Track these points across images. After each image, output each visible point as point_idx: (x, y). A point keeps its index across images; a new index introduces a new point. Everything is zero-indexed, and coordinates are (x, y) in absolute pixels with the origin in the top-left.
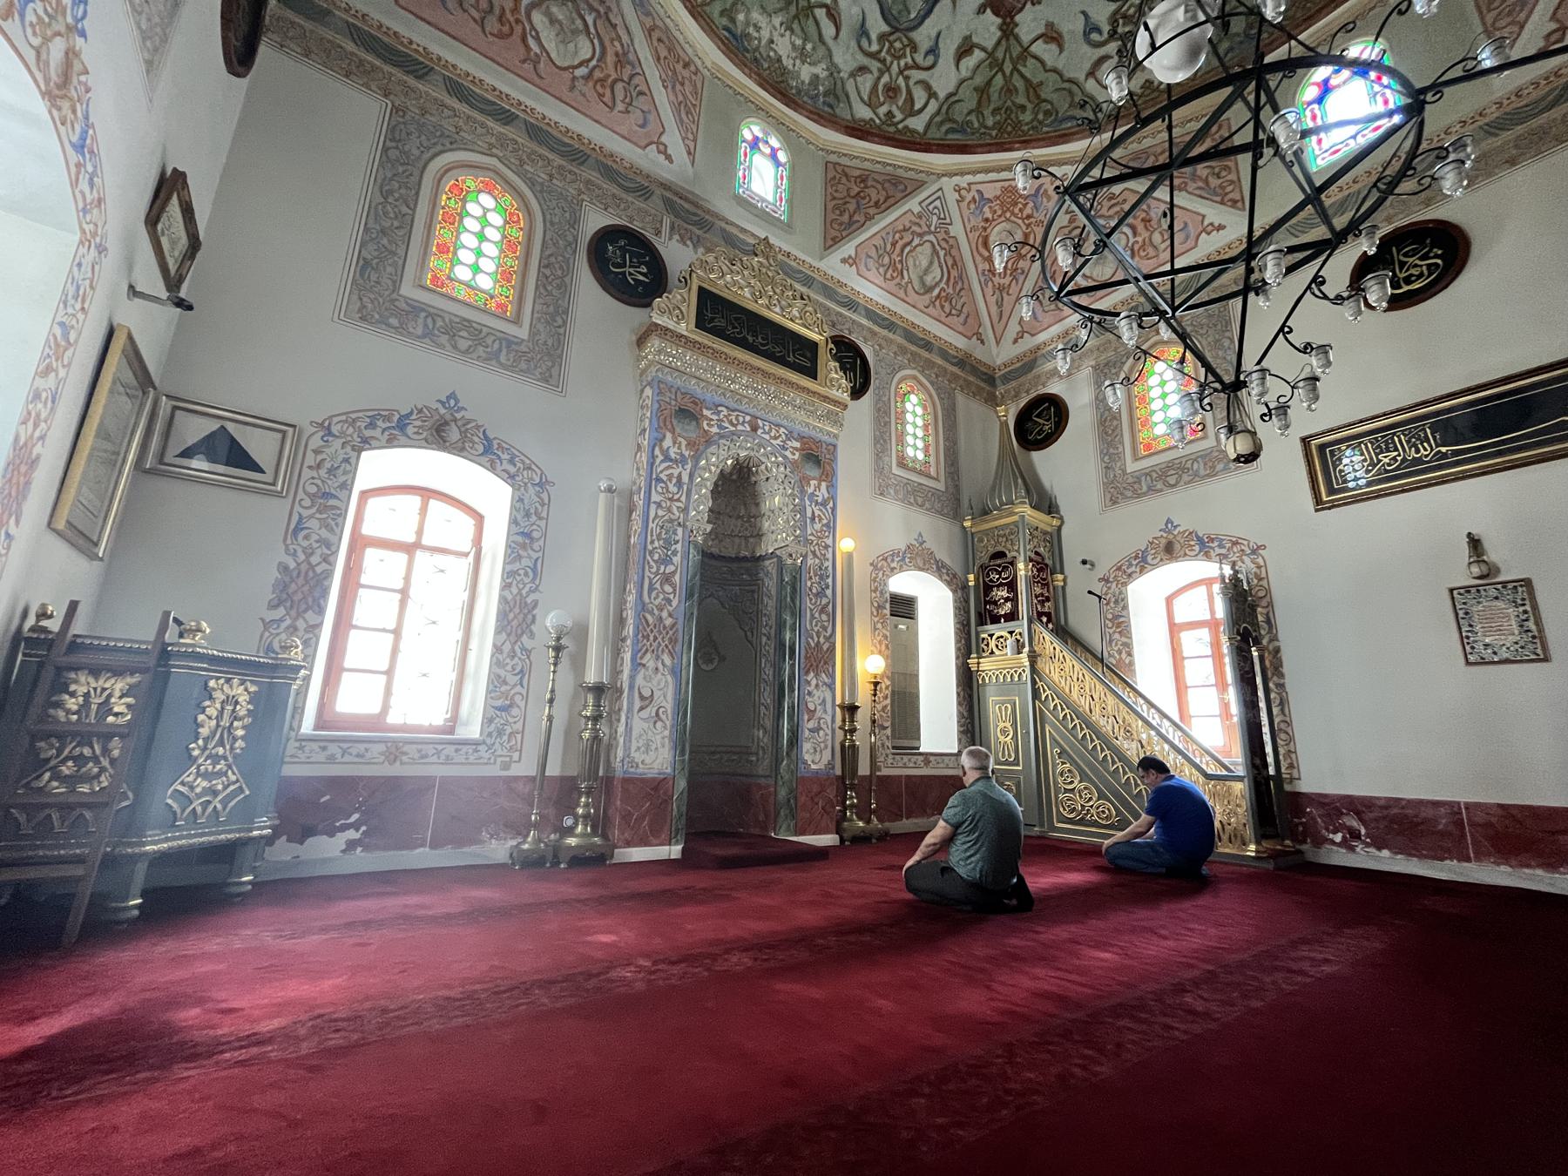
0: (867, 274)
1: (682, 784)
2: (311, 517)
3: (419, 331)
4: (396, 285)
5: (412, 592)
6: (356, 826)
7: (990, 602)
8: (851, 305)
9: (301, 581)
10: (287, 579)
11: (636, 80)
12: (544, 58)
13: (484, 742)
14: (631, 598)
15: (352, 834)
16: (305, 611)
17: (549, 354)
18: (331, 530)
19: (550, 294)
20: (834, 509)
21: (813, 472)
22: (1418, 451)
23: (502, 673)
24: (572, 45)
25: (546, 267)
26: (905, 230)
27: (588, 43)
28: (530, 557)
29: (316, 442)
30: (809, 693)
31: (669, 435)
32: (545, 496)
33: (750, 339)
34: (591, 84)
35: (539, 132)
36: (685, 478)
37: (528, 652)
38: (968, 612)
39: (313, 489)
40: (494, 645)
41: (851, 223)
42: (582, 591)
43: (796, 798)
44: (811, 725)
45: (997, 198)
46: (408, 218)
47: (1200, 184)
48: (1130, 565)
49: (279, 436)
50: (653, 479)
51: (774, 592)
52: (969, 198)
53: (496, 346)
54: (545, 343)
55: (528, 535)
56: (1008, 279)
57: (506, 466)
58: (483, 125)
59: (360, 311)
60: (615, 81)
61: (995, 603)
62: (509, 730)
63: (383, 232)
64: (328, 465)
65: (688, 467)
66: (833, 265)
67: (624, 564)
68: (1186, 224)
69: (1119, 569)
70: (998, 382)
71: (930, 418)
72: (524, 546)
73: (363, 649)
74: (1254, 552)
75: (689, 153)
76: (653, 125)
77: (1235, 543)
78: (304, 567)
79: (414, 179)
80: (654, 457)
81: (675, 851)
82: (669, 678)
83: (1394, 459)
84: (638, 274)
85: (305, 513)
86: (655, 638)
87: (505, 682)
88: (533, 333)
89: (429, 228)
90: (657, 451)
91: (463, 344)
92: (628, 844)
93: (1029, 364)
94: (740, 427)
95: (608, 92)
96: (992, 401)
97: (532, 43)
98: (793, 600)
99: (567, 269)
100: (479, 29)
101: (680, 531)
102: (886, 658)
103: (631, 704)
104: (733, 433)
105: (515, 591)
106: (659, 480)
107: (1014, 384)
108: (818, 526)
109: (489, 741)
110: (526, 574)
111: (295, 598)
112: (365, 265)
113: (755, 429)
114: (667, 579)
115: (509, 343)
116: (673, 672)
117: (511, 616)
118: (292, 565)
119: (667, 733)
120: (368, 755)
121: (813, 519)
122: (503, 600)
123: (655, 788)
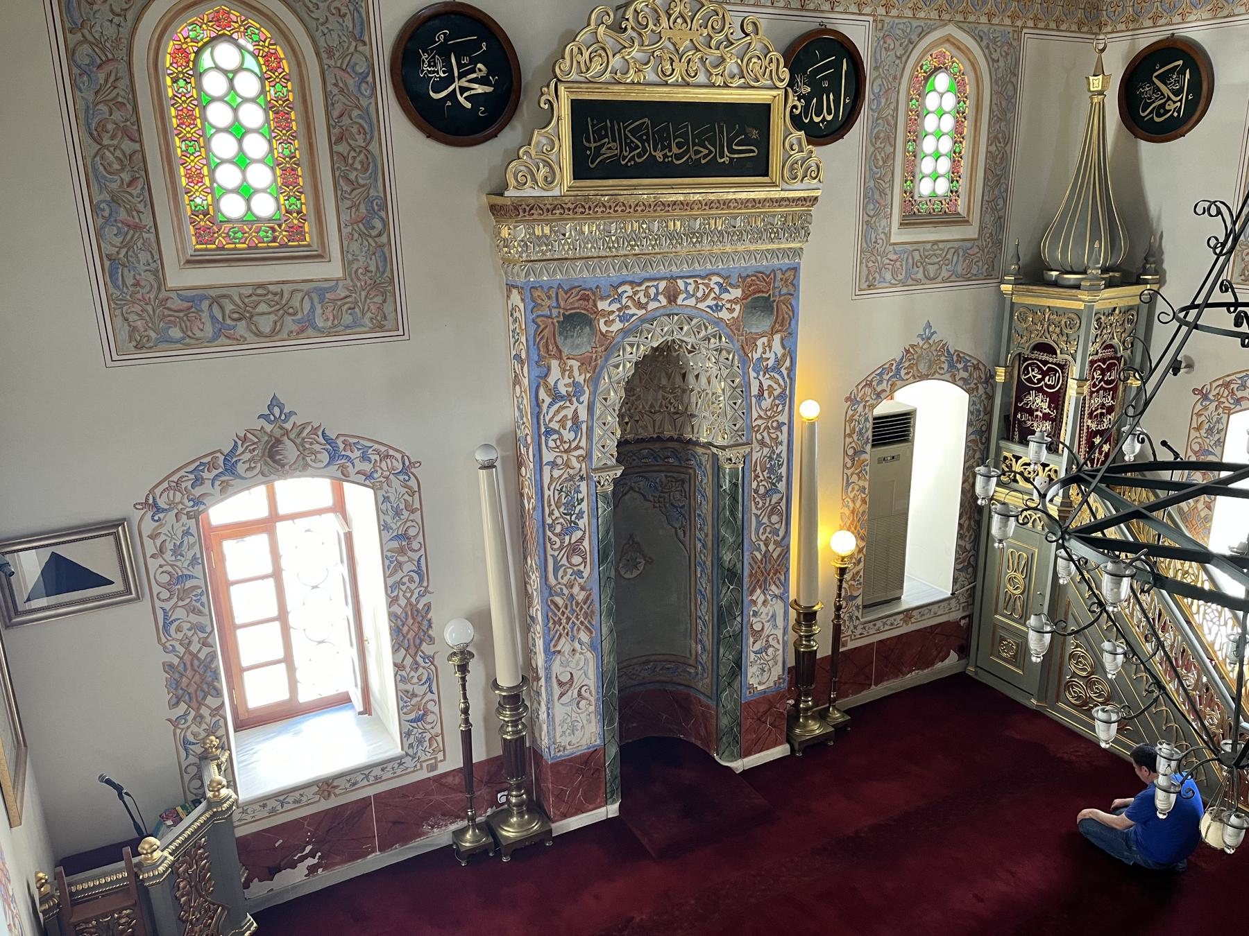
1: (613, 750)
2: (175, 607)
3: (209, 328)
4: (158, 274)
5: (292, 620)
7: (1023, 410)
9: (189, 673)
10: (177, 676)
13: (407, 754)
14: (535, 578)
15: (310, 861)
16: (204, 698)
17: (375, 285)
18: (200, 613)
19: (355, 185)
20: (791, 370)
21: (762, 324)
23: (409, 687)
25: (340, 139)
28: (411, 560)
29: (148, 526)
30: (755, 614)
31: (555, 364)
32: (413, 483)
33: (659, 155)
36: (583, 415)
37: (431, 659)
38: (989, 413)
39: (166, 578)
40: (395, 665)
42: (476, 576)
43: (740, 725)
44: (757, 647)
46: (138, 157)
49: (111, 538)
50: (543, 432)
51: (709, 492)
53: (307, 306)
55: (404, 536)
57: (361, 466)
59: (131, 338)
61: (1031, 412)
62: (428, 736)
63: (115, 200)
64: (169, 546)
65: (585, 398)
67: (522, 535)
69: (1226, 385)
72: (401, 551)
73: (254, 645)
78: (187, 658)
79: (123, 84)
80: (538, 403)
81: (612, 810)
82: (589, 655)
85: (167, 606)
86: (568, 619)
87: (414, 695)
88: (347, 264)
90: (542, 394)
91: (265, 324)
92: (565, 816)
94: (652, 305)
99: (371, 127)
101: (583, 485)
102: (860, 537)
103: (550, 693)
104: (642, 320)
105: (403, 602)
106: (549, 432)
109: (411, 752)
110: (411, 580)
111: (191, 690)
112: (113, 267)
113: (672, 298)
114: (574, 549)
115: (322, 292)
116: (592, 647)
117: (405, 629)
118: (176, 661)
119: (592, 708)
120: (304, 799)
122: (392, 616)
123: (587, 763)
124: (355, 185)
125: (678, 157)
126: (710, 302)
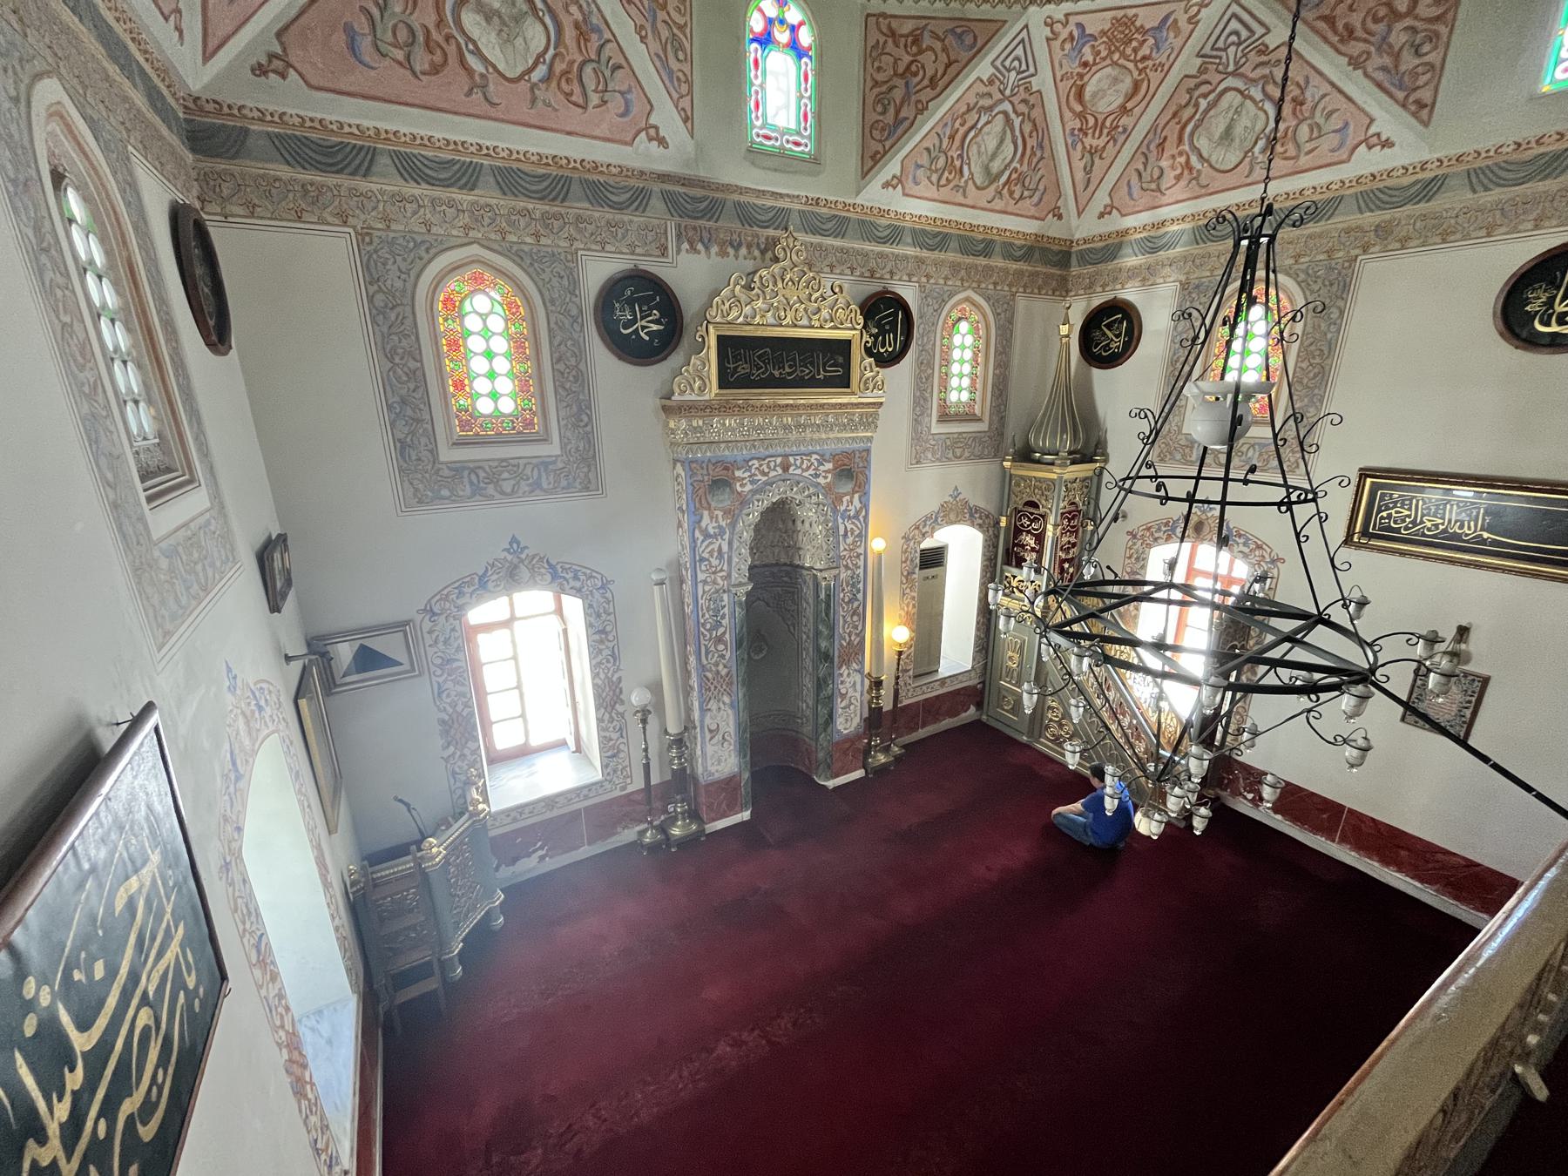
0: (916, 190)
1: (746, 775)
2: (445, 681)
4: (434, 452)
6: (541, 848)
7: (1017, 545)
8: (894, 235)
11: (607, 52)
12: (492, 77)
15: (541, 853)
19: (569, 392)
20: (866, 517)
22: (1461, 527)
24: (519, 42)
26: (969, 110)
27: (539, 27)
29: (427, 625)
31: (706, 513)
32: (609, 595)
33: (776, 373)
34: (554, 84)
35: (511, 178)
36: (725, 548)
38: (996, 547)
39: (439, 661)
41: (898, 122)
42: (652, 652)
45: (1104, 33)
47: (1387, 60)
48: (1159, 530)
50: (697, 560)
52: (1064, 34)
54: (577, 450)
56: (1104, 139)
57: (572, 583)
58: (451, 204)
60: (583, 64)
61: (1023, 546)
63: (403, 402)
65: (726, 537)
66: (875, 195)
67: (684, 633)
68: (1347, 124)
70: (1074, 260)
71: (981, 344)
72: (601, 642)
73: (499, 706)
74: (1273, 561)
75: (685, 121)
76: (638, 107)
77: (1259, 547)
79: (408, 322)
80: (694, 540)
83: (1437, 526)
84: (649, 326)
85: (441, 680)
88: (563, 446)
89: (440, 369)
90: (697, 534)
93: (1108, 250)
94: (773, 474)
95: (577, 89)
96: (1062, 288)
97: (472, 60)
98: (827, 615)
99: (580, 353)
100: (408, 73)
101: (725, 596)
103: (703, 738)
104: (766, 483)
106: (702, 560)
107: (1091, 269)
108: (850, 540)
113: (786, 468)
114: (719, 640)
115: (546, 465)
116: (732, 706)
121: (845, 535)
123: (729, 784)
124: (569, 392)
125: (790, 374)
126: (811, 472)
